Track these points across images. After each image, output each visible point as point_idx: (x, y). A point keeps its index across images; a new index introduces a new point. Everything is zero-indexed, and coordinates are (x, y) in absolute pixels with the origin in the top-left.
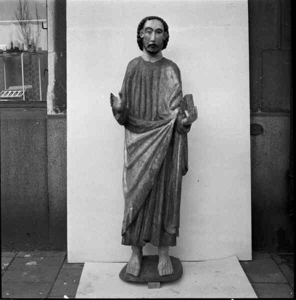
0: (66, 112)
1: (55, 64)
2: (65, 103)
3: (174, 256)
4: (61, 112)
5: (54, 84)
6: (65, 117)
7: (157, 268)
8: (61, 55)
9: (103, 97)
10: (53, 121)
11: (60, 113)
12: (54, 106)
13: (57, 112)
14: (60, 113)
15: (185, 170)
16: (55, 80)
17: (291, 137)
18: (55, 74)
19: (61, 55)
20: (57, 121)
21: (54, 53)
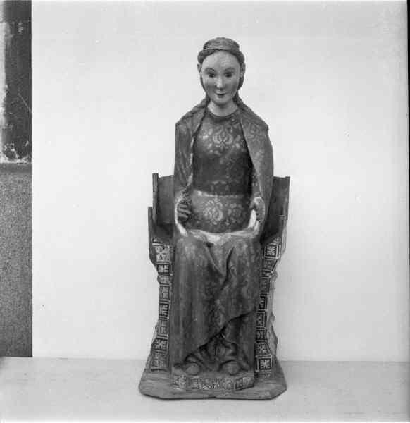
0: (30, 160)
1: (6, 50)
2: (28, 137)
3: (287, 378)
4: (20, 158)
5: (5, 94)
6: (28, 169)
7: (283, 178)
8: (21, 30)
9: (97, 41)
10: (244, 326)
11: (18, 161)
12: (6, 144)
13: (11, 156)
14: (18, 161)
15: (276, 342)
16: (7, 86)
17: (148, 360)
18: (7, 72)
19: (21, 30)
20: (11, 177)
21: (5, 23)
